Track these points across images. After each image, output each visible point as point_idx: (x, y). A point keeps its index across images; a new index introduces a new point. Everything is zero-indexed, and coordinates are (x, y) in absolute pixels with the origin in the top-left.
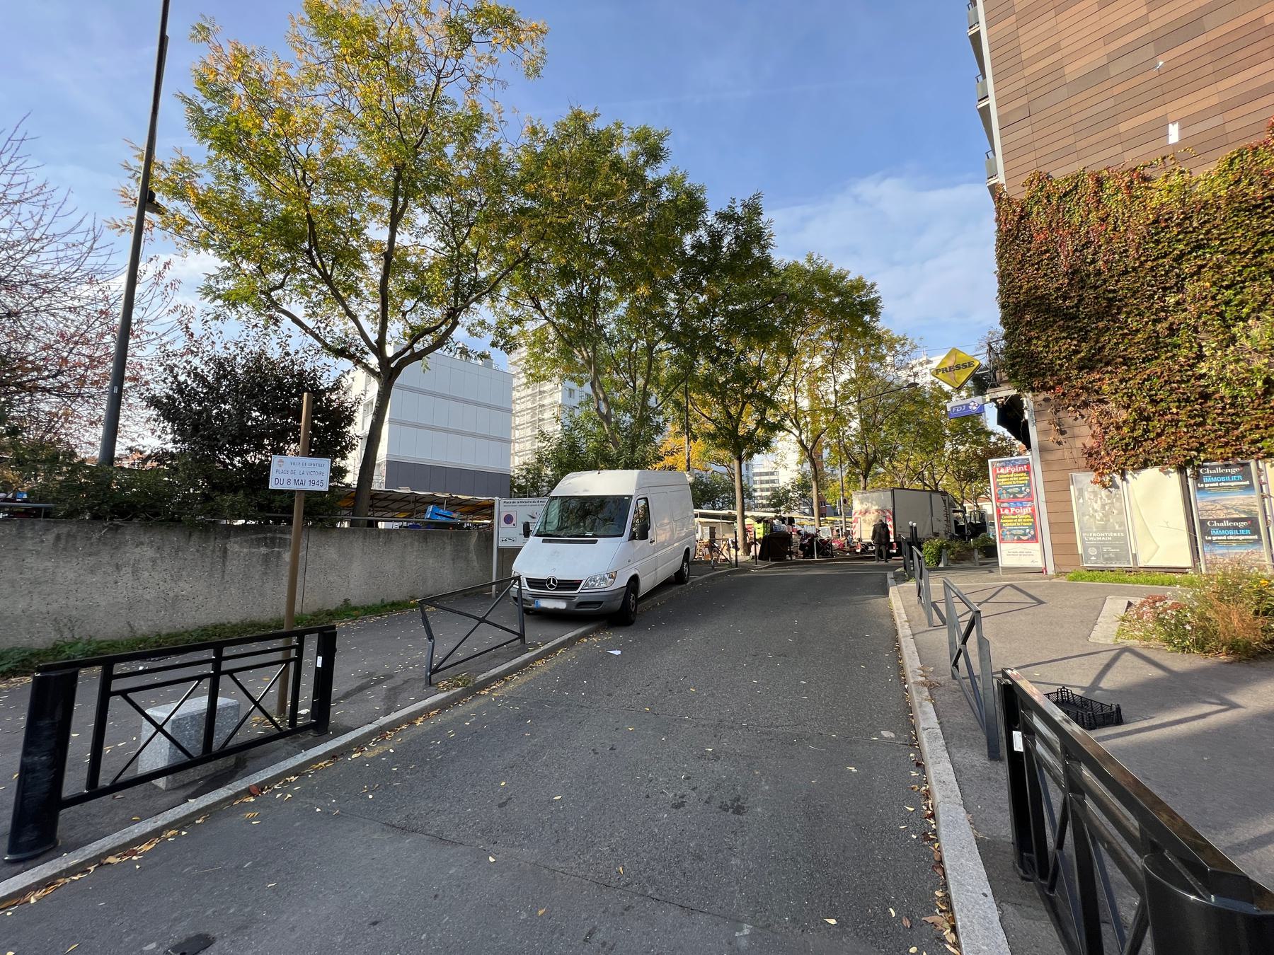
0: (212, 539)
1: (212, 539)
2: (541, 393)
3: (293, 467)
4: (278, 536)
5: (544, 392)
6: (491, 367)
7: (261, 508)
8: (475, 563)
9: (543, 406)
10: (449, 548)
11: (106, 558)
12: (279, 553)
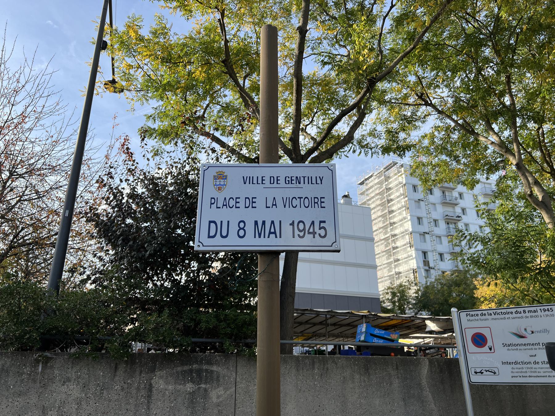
0: (138, 373)
1: (138, 373)
2: (392, 224)
3: (251, 190)
4: (205, 367)
5: (394, 223)
6: (351, 204)
7: (187, 331)
8: (433, 406)
9: (395, 235)
10: (396, 383)
11: (34, 399)
12: (206, 390)
